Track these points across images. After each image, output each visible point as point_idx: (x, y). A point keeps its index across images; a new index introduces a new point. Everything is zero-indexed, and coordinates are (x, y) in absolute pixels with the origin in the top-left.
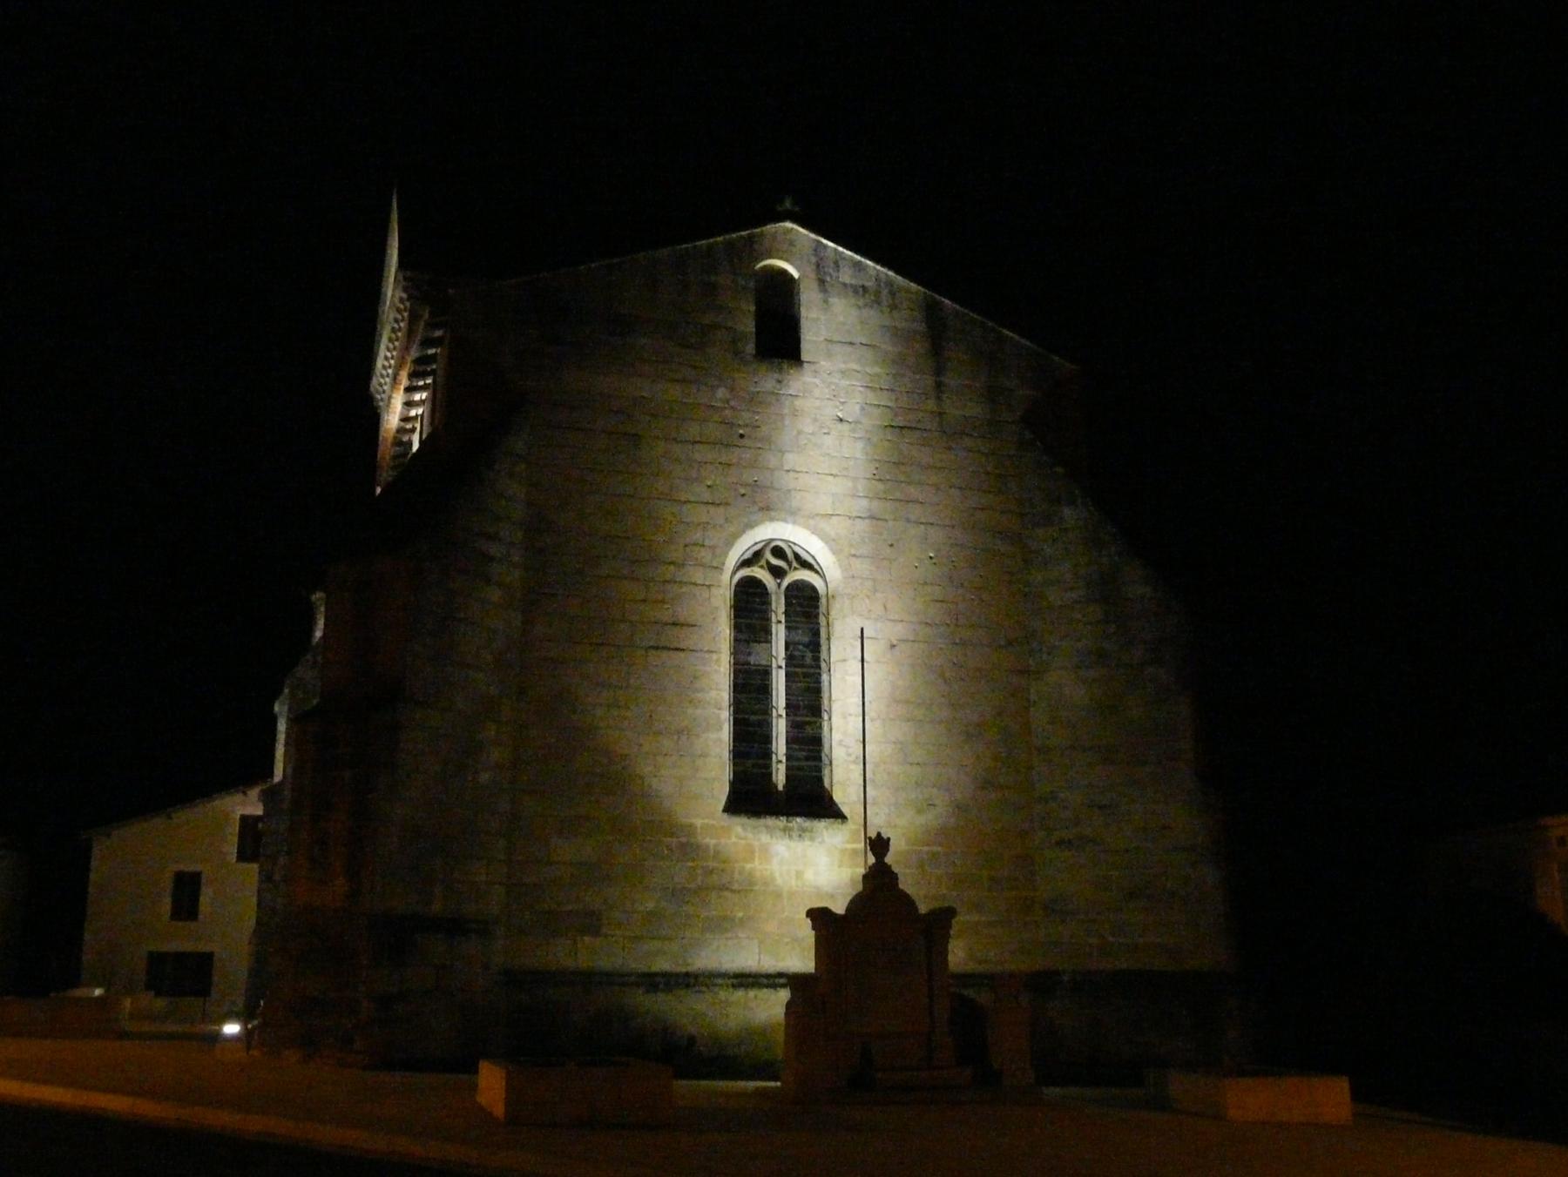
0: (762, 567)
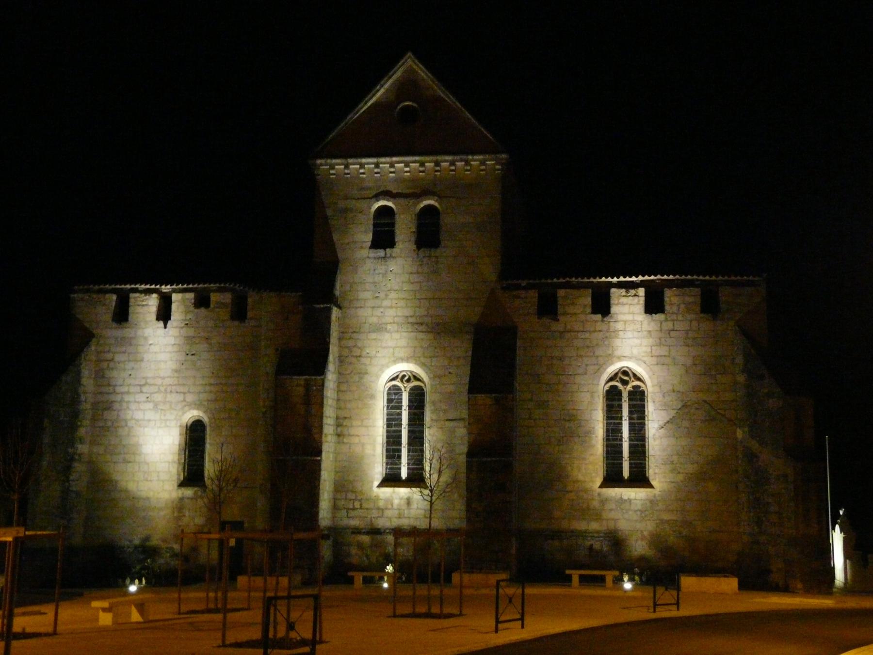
0: (617, 381)
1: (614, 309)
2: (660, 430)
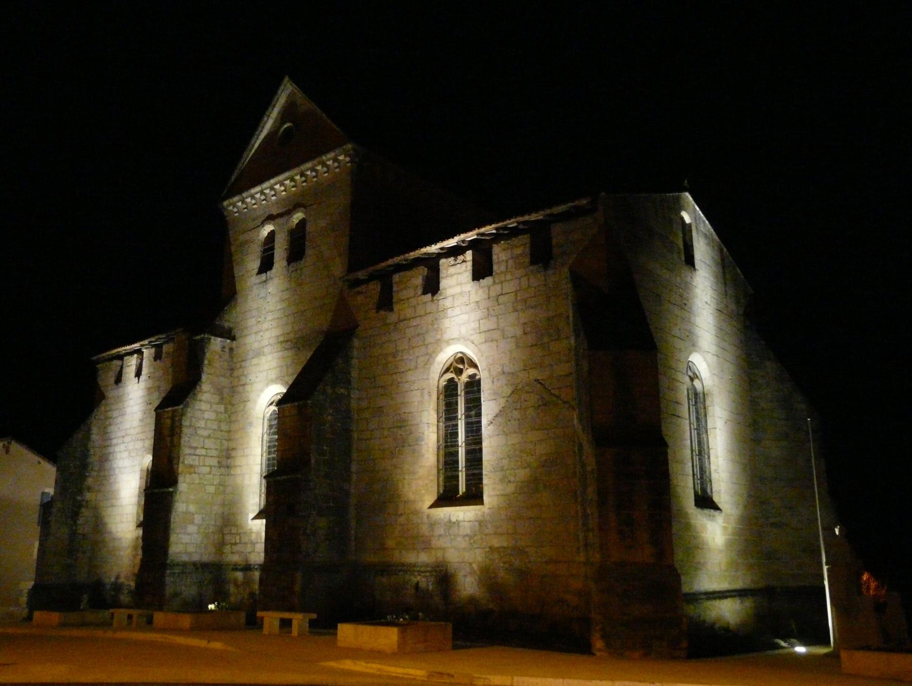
1: (443, 283)
2: (489, 427)
